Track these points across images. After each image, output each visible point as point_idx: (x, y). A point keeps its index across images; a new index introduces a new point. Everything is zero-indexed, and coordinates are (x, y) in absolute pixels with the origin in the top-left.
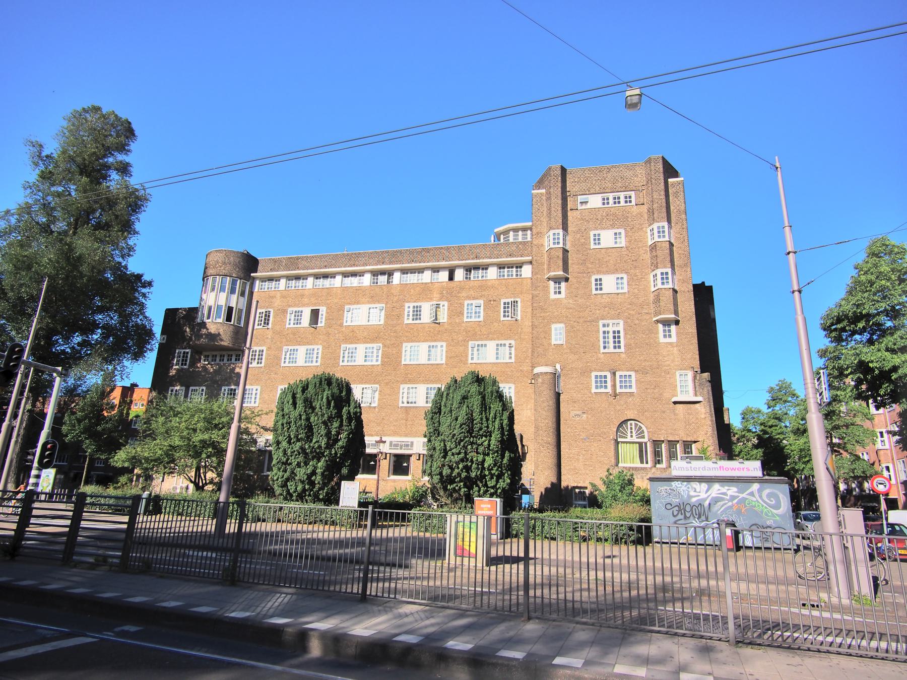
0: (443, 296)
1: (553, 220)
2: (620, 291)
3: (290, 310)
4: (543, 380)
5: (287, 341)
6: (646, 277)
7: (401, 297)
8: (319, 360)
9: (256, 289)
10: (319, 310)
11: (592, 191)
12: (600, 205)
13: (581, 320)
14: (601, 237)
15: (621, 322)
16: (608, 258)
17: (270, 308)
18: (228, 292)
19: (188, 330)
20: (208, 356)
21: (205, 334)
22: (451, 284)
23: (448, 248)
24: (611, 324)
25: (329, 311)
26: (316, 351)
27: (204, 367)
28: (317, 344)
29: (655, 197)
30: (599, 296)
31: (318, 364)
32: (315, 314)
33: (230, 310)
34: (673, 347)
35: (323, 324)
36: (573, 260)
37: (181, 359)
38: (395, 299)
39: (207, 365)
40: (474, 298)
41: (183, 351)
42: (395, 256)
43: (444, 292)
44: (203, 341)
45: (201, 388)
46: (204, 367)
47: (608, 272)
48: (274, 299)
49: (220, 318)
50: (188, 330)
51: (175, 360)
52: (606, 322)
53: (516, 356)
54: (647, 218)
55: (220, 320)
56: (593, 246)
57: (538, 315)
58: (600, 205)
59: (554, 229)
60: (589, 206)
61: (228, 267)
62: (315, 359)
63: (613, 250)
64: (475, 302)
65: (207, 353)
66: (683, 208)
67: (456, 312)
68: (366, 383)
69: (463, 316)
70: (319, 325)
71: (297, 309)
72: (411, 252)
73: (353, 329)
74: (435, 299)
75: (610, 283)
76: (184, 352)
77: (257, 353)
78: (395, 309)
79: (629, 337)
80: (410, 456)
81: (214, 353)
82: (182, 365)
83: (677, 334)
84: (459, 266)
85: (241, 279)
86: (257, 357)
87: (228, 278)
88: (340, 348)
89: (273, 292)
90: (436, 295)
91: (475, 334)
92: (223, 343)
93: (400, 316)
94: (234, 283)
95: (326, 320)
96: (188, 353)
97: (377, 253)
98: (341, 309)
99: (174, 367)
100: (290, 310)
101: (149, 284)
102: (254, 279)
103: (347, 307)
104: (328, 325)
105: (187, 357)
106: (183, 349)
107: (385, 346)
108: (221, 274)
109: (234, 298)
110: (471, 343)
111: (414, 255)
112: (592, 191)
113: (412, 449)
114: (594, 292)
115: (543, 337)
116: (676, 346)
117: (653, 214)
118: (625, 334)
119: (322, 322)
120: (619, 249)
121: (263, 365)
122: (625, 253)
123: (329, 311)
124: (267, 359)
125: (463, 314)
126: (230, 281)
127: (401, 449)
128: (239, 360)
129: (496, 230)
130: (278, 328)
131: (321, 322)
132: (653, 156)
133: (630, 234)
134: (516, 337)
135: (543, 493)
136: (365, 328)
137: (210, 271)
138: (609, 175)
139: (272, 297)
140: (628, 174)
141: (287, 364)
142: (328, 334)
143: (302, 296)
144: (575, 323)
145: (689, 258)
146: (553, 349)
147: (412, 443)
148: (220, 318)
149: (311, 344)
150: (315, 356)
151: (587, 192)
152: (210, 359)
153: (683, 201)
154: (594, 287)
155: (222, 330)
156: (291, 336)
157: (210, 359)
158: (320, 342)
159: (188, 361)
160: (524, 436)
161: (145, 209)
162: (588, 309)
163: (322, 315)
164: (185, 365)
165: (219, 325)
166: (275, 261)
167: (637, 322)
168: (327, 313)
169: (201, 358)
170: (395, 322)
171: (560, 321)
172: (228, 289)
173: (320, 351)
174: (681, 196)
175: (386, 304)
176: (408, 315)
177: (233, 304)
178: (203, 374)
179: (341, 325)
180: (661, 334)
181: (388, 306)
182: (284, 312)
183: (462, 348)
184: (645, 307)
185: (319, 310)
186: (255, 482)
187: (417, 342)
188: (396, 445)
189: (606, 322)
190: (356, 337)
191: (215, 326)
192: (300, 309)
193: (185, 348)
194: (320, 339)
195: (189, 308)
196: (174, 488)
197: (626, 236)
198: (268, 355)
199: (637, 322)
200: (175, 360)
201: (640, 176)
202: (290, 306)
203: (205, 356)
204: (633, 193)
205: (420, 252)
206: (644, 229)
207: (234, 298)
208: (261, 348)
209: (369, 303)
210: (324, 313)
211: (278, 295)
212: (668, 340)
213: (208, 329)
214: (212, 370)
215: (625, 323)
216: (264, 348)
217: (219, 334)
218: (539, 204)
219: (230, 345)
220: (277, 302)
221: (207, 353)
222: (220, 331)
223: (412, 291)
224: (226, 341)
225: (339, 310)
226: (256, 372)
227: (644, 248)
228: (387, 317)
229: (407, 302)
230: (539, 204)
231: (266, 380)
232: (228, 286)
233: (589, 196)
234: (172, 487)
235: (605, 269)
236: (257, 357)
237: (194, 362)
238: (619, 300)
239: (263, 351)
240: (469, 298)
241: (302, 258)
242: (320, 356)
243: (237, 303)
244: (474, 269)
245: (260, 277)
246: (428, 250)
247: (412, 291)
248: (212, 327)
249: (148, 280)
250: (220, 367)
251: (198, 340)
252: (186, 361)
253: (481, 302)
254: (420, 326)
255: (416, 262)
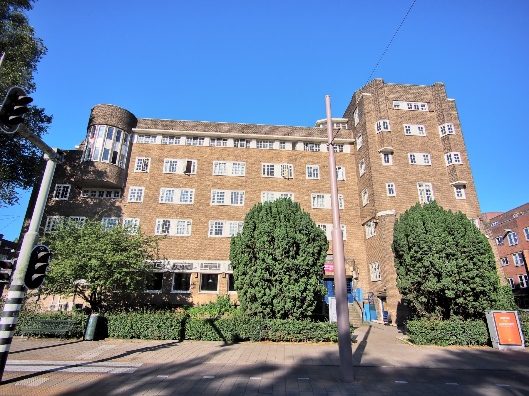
0: (290, 160)
1: (382, 113)
2: (427, 164)
3: (166, 160)
4: (390, 220)
5: (164, 183)
6: (441, 156)
7: (258, 158)
8: (193, 199)
9: (135, 141)
10: (191, 162)
11: (402, 99)
12: (406, 108)
13: (405, 181)
14: (418, 129)
15: (431, 185)
16: (417, 142)
17: (149, 157)
18: (114, 140)
19: (68, 168)
20: (88, 192)
21: (93, 171)
22: (294, 152)
23: (291, 128)
24: (424, 185)
25: (200, 163)
26: (189, 193)
27: (84, 200)
28: (191, 188)
29: (443, 107)
30: (414, 166)
31: (192, 203)
32: (189, 164)
33: (115, 154)
34: (464, 202)
35: (195, 173)
36: (394, 141)
37: (61, 192)
38: (254, 159)
39: (87, 198)
40: (312, 164)
41: (63, 186)
42: (252, 129)
43: (291, 157)
44: (91, 176)
45: (81, 218)
46: (84, 200)
47: (417, 151)
48: (152, 151)
49: (107, 159)
50: (68, 168)
51: (55, 192)
52: (421, 183)
53: (345, 205)
54: (437, 120)
55: (108, 161)
56: (406, 134)
57: (376, 175)
58: (406, 108)
59: (383, 119)
60: (400, 108)
61: (115, 120)
62: (189, 199)
63: (420, 138)
64: (313, 167)
65: (86, 189)
66: (457, 117)
67: (300, 172)
68: (233, 219)
69: (305, 175)
70: (192, 173)
71: (173, 160)
72: (264, 127)
73: (221, 178)
74: (284, 161)
75: (420, 159)
76: (64, 187)
77: (136, 192)
78: (254, 166)
79: (436, 194)
80: (190, 274)
81: (94, 189)
82: (62, 197)
83: (466, 194)
84: (300, 141)
85: (124, 131)
86: (136, 195)
87: (115, 128)
88: (211, 192)
89: (151, 145)
90: (284, 159)
91: (315, 188)
92: (109, 180)
93: (257, 172)
94: (119, 133)
95: (198, 170)
96: (68, 187)
97: (238, 125)
98: (210, 162)
99: (54, 199)
100: (166, 160)
101: (49, 120)
102: (133, 133)
103: (215, 162)
104: (200, 174)
105: (67, 191)
106: (63, 184)
107: (247, 192)
108: (109, 124)
109: (119, 145)
110: (312, 195)
111: (266, 129)
112: (402, 99)
113: (219, 270)
114: (411, 163)
115: (381, 190)
116: (466, 202)
117: (444, 117)
118: (434, 192)
119: (194, 172)
120: (423, 138)
121: (142, 201)
122: (427, 140)
123: (200, 163)
124: (145, 197)
125: (305, 174)
126: (116, 131)
127: (210, 269)
128: (118, 196)
129: (318, 121)
130: (155, 173)
131: (194, 171)
132: (439, 83)
133: (428, 129)
134: (344, 192)
135: (400, 302)
136: (231, 177)
137: (96, 121)
138: (411, 91)
139: (150, 149)
140: (423, 92)
141: (164, 202)
142: (200, 181)
143: (177, 150)
144: (401, 183)
145: (465, 148)
146: (388, 199)
147: (219, 265)
148: (107, 159)
149: (186, 188)
150: (189, 196)
151: (398, 99)
152: (89, 194)
153: (456, 113)
154: (410, 160)
155: (108, 169)
156: (168, 180)
157: (89, 194)
158: (193, 186)
159: (68, 194)
160: (355, 261)
161: (39, 59)
162: (409, 174)
163: (194, 166)
164: (65, 197)
165: (106, 165)
166: (152, 122)
167: (440, 185)
168: (198, 164)
169: (80, 193)
170: (254, 175)
171: (391, 180)
172: (114, 137)
173: (193, 193)
174: (455, 109)
175: (247, 162)
176: (264, 171)
177: (118, 150)
178: (83, 205)
179: (211, 174)
180: (456, 194)
181: (248, 163)
182: (161, 161)
183: (306, 198)
184: (444, 175)
185: (191, 162)
186: (135, 299)
187: (272, 191)
188: (206, 267)
189: (421, 183)
190: (223, 184)
191: (102, 165)
192: (175, 160)
193: (65, 183)
194: (193, 184)
195: (71, 151)
196: (53, 307)
197: (426, 130)
198: (146, 193)
199: (440, 185)
200: (55, 192)
201: (429, 94)
202: (166, 157)
203: (85, 192)
204: (426, 104)
205: (270, 128)
206: (436, 127)
207: (119, 145)
208: (140, 188)
209: (233, 160)
210: (196, 165)
211: (156, 148)
212: (460, 198)
213: (96, 167)
214: (92, 203)
215: (433, 185)
216: (143, 189)
217: (106, 172)
218: (368, 102)
219: (115, 183)
220: (155, 153)
221: (86, 189)
222: (107, 170)
223: (266, 154)
224: (111, 179)
225: (208, 163)
226: (136, 207)
227: (438, 139)
228: (248, 171)
229: (263, 162)
230: (368, 102)
231: (145, 214)
232: (114, 134)
233: (400, 102)
234: (49, 305)
235: (416, 149)
236: (136, 195)
237: (74, 196)
238: (427, 169)
239: (141, 190)
240: (308, 163)
241: (176, 122)
242: (193, 196)
243: (121, 149)
244: (310, 143)
245: (140, 132)
246: (277, 128)
247: (266, 154)
248: (100, 166)
249: (48, 116)
250: (101, 201)
251: (85, 176)
252: (66, 194)
253: (318, 167)
254: (274, 179)
255: (268, 134)
